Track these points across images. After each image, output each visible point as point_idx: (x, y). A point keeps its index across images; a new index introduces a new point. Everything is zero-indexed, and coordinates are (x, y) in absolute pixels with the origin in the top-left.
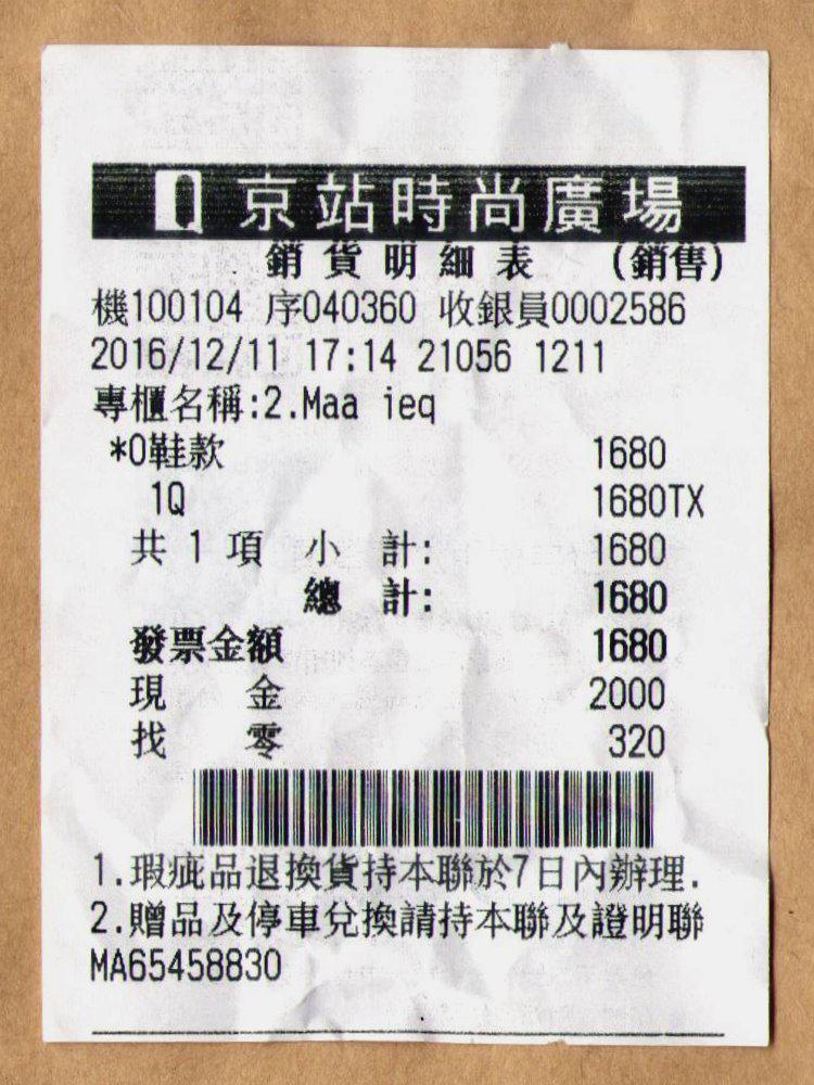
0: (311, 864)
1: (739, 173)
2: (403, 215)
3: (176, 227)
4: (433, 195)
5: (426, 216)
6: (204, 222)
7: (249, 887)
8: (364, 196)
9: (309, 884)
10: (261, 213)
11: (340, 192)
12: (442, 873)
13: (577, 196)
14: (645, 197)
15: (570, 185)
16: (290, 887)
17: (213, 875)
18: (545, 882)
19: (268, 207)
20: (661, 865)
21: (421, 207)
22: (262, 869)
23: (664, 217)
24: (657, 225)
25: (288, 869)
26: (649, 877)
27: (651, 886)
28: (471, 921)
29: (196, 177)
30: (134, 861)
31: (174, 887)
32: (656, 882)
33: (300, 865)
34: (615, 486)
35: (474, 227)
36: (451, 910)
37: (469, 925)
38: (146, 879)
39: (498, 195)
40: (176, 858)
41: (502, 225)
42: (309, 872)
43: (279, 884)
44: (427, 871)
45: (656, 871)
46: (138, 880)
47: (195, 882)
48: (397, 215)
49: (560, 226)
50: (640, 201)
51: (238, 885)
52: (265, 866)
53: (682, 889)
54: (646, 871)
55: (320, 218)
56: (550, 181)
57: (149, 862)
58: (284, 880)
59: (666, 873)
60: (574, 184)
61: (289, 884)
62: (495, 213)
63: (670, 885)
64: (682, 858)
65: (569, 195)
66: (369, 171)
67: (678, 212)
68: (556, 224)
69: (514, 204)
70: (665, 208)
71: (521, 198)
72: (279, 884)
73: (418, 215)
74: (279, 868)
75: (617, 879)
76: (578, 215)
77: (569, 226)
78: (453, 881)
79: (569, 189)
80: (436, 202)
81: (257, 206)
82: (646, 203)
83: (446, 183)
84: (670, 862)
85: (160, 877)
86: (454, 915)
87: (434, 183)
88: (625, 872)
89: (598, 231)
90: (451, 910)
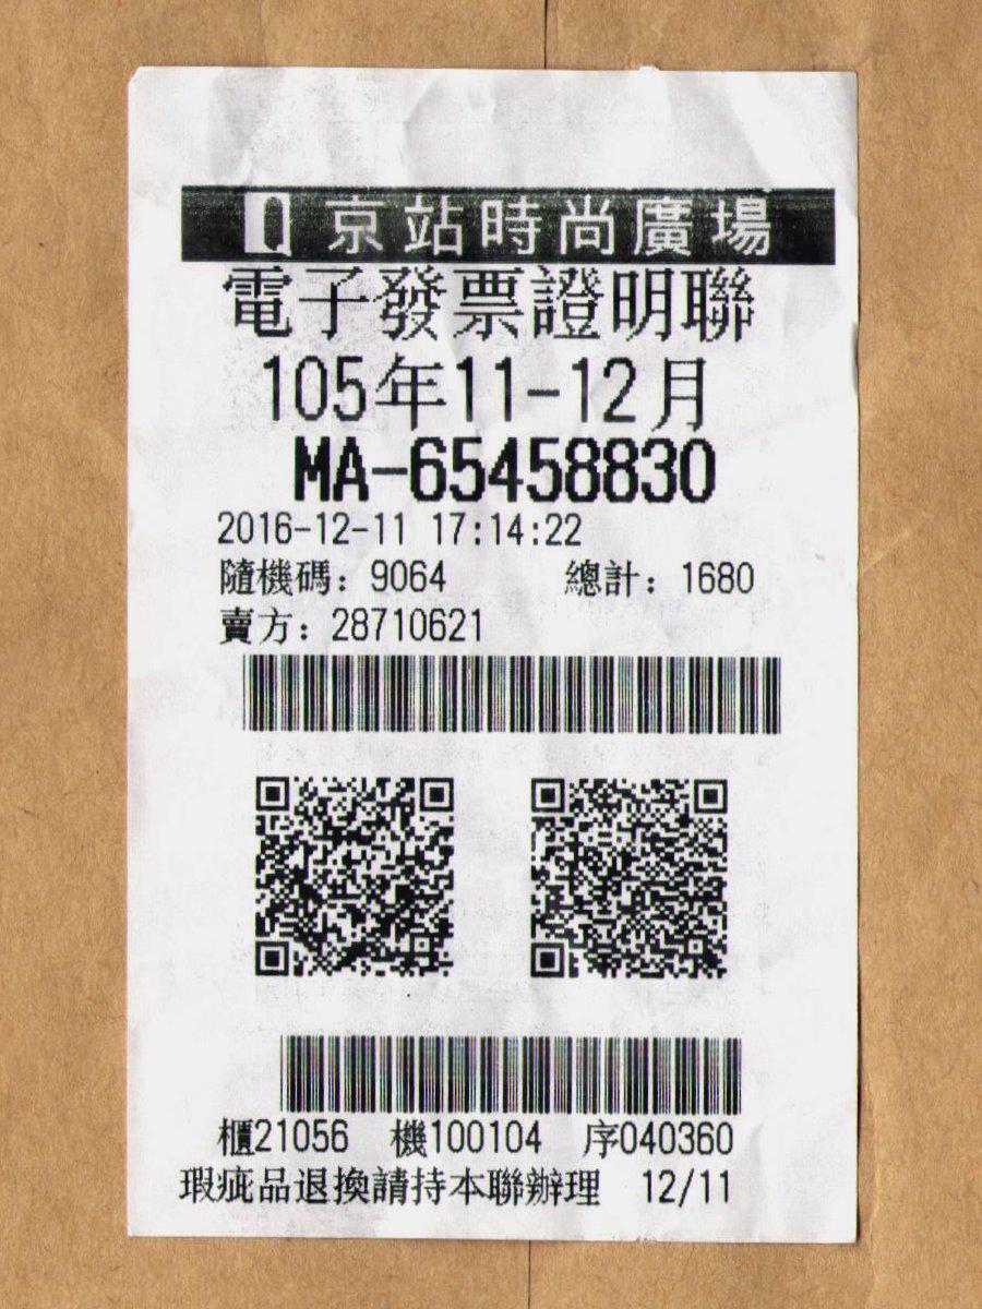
0: (359, 1178)
1: (828, 195)
2: (493, 237)
3: (266, 250)
4: (523, 217)
5: (515, 239)
6: (293, 247)
7: (298, 1201)
8: (453, 218)
9: (357, 1198)
10: (349, 236)
11: (428, 214)
12: (492, 1187)
13: (666, 218)
14: (733, 219)
15: (659, 207)
16: (338, 1201)
17: (262, 1188)
18: (270, 1177)
19: (356, 230)
20: (577, 1179)
21: (511, 230)
22: (310, 1183)
23: (752, 239)
24: (746, 247)
25: (336, 1183)
26: (565, 1191)
27: (567, 1200)
28: (443, 1188)
29: (285, 200)
30: (183, 1174)
31: (223, 1201)
32: (572, 1196)
33: (348, 1180)
34: (704, 564)
35: (563, 250)
36: (423, 1176)
37: (442, 1192)
38: (195, 1192)
39: (587, 217)
40: (225, 1172)
41: (592, 247)
42: (357, 1186)
43: (327, 1198)
44: (477, 1184)
45: (572, 1184)
46: (187, 1193)
47: (244, 1195)
48: (486, 239)
49: (650, 249)
50: (729, 223)
51: (287, 1199)
52: (313, 1180)
53: (597, 1203)
54: (561, 1186)
55: (409, 241)
56: (640, 204)
57: (198, 1176)
58: (332, 1194)
59: (582, 1188)
60: (664, 206)
61: (337, 1197)
62: (585, 235)
63: (585, 1200)
64: (597, 1172)
65: (659, 217)
66: (457, 193)
67: (767, 234)
68: (645, 247)
69: (604, 227)
70: (754, 230)
71: (610, 220)
72: (327, 1198)
73: (507, 236)
74: (327, 1183)
75: (533, 1193)
76: (668, 238)
77: (659, 249)
78: (503, 1195)
79: (658, 211)
80: (526, 225)
81: (346, 229)
82: (734, 226)
83: (536, 206)
84: (585, 1176)
85: (209, 1190)
86: (428, 1182)
87: (523, 204)
88: (542, 1186)
89: (688, 253)
90: (423, 1176)
